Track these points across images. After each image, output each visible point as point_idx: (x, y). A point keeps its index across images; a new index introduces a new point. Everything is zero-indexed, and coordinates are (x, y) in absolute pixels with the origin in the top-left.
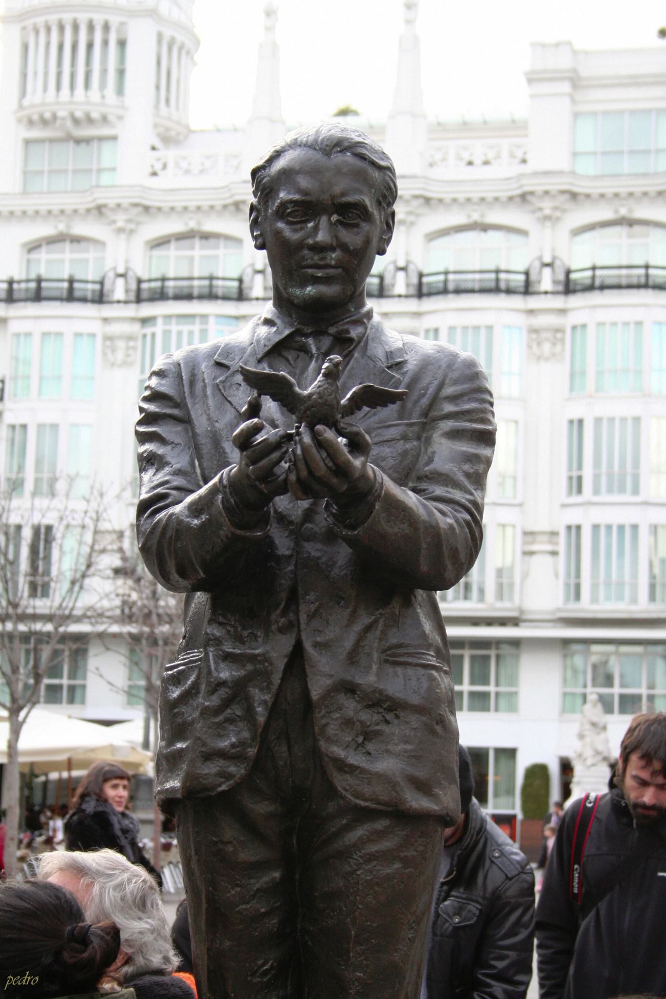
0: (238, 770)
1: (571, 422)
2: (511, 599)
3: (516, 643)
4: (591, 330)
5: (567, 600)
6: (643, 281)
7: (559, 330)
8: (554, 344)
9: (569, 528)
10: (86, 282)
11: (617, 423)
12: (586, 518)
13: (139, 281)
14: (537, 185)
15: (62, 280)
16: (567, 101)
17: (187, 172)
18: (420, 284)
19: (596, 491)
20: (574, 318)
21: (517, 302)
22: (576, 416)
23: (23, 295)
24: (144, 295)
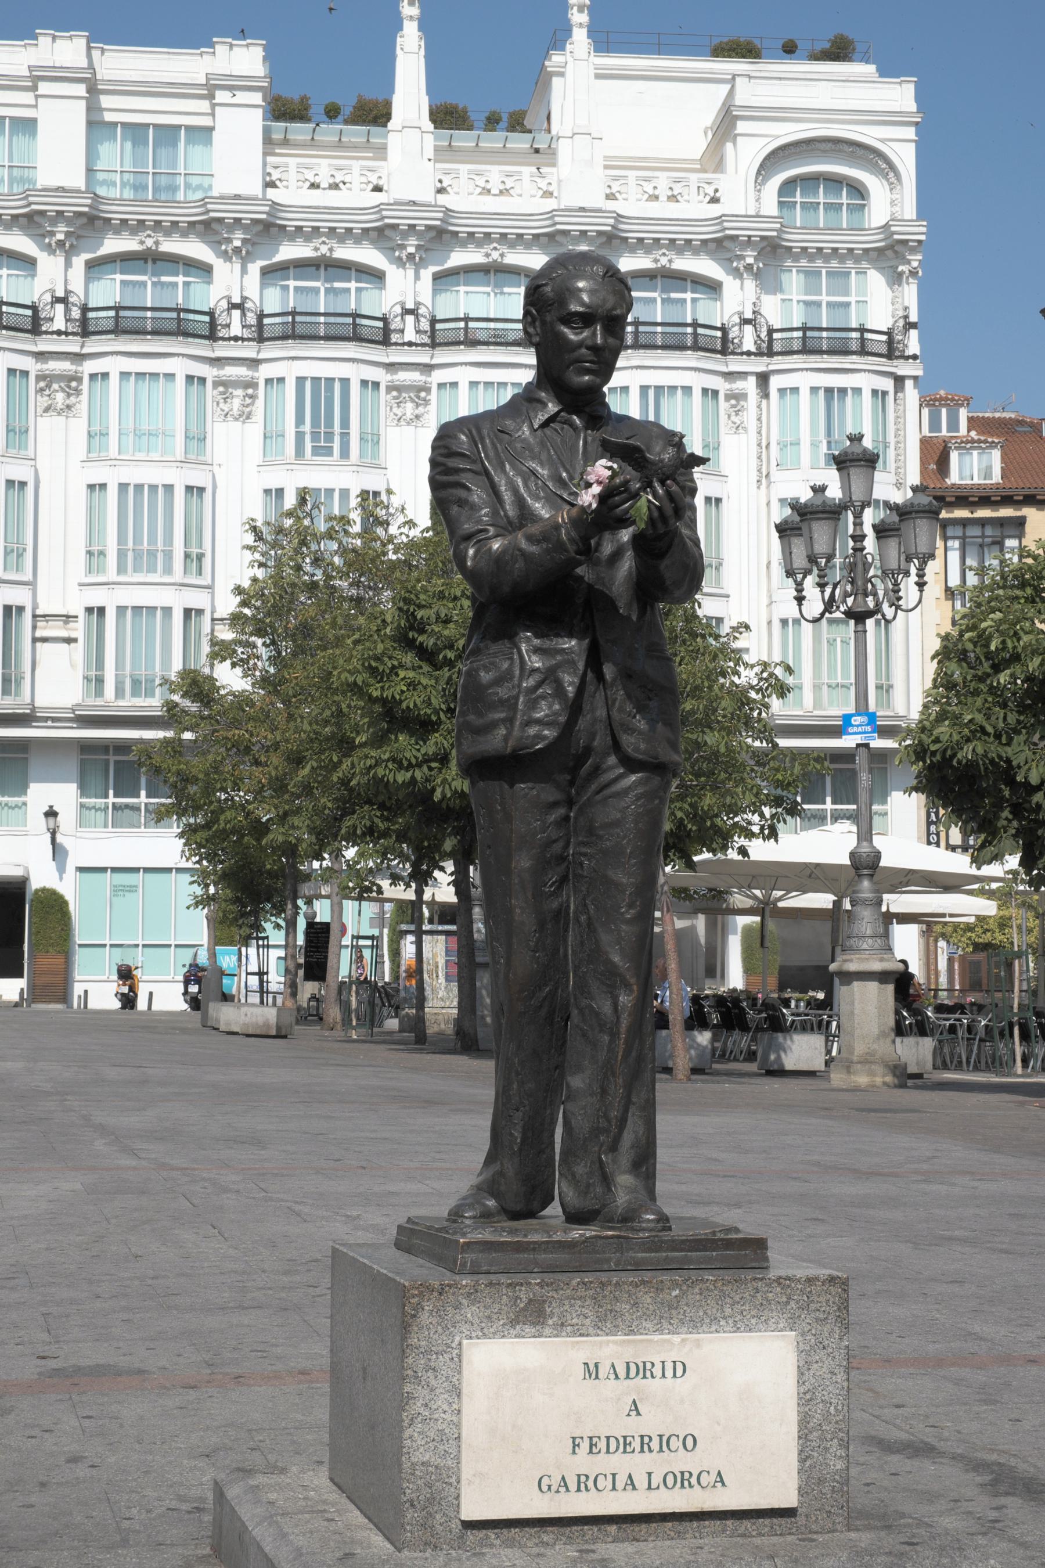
1: (267, 492)
2: (18, 694)
3: (23, 745)
4: (114, 379)
5: (87, 693)
6: (174, 326)
7: (252, 384)
8: (69, 395)
9: (89, 610)
10: (319, 314)
11: (131, 489)
12: (110, 599)
13: (771, 331)
14: (402, 218)
15: (686, 325)
16: (83, 103)
17: (314, 186)
18: (260, 325)
19: (121, 569)
20: (266, 371)
21: (201, 348)
22: (273, 485)
23: (278, 331)
24: (777, 347)
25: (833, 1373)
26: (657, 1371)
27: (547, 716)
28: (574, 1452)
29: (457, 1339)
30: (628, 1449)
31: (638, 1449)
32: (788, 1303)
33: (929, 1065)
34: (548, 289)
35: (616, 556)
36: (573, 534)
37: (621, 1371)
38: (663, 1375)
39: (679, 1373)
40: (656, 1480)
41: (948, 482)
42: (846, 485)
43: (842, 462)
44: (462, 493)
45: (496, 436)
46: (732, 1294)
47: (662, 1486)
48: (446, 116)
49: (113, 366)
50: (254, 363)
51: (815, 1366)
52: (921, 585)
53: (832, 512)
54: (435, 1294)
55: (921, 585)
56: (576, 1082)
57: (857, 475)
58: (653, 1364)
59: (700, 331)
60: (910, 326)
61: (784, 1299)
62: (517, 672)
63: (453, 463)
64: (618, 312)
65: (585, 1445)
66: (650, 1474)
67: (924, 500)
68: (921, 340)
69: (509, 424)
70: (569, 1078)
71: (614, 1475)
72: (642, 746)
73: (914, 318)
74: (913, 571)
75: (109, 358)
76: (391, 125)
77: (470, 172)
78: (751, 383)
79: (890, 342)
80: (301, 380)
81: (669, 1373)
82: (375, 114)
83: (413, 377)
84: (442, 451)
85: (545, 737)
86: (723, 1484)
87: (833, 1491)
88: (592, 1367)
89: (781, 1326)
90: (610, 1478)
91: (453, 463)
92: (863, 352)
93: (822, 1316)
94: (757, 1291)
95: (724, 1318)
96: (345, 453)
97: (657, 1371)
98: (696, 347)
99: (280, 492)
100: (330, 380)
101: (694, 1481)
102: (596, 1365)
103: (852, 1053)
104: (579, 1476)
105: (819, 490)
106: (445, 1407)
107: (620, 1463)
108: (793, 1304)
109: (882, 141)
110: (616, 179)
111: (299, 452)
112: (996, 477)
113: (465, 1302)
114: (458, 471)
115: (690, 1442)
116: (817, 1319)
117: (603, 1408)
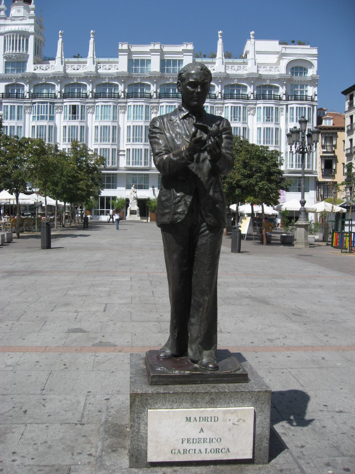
0: (183, 217)
6: (176, 96)
17: (43, 70)
20: (258, 106)
25: (265, 419)
26: (209, 420)
27: (181, 211)
28: (182, 443)
29: (147, 409)
30: (189, 442)
31: (203, 442)
32: (252, 398)
34: (184, 74)
35: (204, 160)
36: (187, 153)
37: (198, 419)
38: (211, 421)
39: (216, 420)
40: (208, 450)
41: (322, 125)
42: (301, 126)
43: (300, 122)
44: (157, 140)
45: (168, 121)
46: (234, 396)
47: (210, 453)
48: (228, 55)
49: (164, 104)
50: (223, 104)
51: (260, 417)
52: (316, 147)
53: (298, 132)
54: (140, 396)
55: (316, 147)
56: (193, 320)
57: (303, 124)
58: (208, 418)
60: (315, 95)
61: (251, 397)
62: (172, 197)
63: (154, 130)
64: (206, 81)
65: (186, 441)
66: (206, 449)
67: (316, 130)
68: (318, 98)
69: (173, 117)
70: (191, 319)
71: (195, 450)
72: (212, 221)
73: (316, 94)
74: (314, 144)
76: (216, 58)
78: (285, 107)
79: (312, 98)
81: (213, 420)
82: (214, 56)
83: (221, 105)
84: (152, 127)
85: (180, 218)
86: (229, 452)
87: (264, 452)
88: (188, 418)
89: (249, 405)
90: (194, 451)
91: (154, 130)
92: (306, 100)
93: (263, 402)
94: (242, 395)
95: (231, 403)
96: (240, 120)
97: (209, 420)
98: (242, 99)
100: (237, 107)
101: (220, 451)
102: (190, 418)
104: (184, 450)
105: (295, 127)
106: (143, 429)
107: (197, 446)
108: (253, 399)
109: (311, 60)
112: (331, 125)
113: (149, 398)
114: (156, 133)
115: (219, 440)
116: (261, 403)
117: (192, 431)
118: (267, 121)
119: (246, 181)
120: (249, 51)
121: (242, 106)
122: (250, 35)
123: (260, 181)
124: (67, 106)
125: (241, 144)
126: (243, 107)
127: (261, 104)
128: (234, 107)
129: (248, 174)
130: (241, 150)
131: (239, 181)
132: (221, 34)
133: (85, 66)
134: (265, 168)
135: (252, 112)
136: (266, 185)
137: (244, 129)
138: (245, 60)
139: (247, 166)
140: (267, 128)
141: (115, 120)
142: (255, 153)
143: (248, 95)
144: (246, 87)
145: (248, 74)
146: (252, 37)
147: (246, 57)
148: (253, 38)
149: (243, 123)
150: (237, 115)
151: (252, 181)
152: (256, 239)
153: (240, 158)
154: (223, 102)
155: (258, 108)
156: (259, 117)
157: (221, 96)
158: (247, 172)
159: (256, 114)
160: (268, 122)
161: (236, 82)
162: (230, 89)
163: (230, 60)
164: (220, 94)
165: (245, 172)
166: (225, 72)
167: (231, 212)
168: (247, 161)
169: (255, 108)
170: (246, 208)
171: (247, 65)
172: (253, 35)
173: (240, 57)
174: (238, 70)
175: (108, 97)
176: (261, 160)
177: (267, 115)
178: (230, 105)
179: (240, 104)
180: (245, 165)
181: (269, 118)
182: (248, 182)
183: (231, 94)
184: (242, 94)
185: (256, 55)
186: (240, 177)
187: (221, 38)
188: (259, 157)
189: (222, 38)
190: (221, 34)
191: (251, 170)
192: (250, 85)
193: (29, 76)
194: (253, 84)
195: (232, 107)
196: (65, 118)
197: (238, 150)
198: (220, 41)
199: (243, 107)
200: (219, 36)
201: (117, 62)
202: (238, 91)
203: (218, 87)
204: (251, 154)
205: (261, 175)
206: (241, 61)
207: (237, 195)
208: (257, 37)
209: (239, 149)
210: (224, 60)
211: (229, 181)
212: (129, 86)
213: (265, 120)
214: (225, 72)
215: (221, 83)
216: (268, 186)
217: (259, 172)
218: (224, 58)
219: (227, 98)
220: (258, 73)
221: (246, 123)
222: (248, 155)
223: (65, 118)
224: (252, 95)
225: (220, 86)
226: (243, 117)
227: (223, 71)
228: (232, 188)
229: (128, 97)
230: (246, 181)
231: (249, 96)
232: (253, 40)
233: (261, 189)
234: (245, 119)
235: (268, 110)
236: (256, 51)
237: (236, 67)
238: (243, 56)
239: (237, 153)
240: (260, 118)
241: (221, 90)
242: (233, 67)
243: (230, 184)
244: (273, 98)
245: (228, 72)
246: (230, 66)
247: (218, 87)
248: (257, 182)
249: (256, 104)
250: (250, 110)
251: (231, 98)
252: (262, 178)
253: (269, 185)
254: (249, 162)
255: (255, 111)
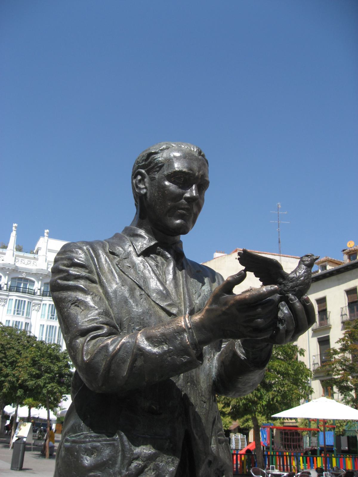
15: (15, 287)
17: (24, 263)
20: (43, 302)
33: (18, 435)
50: (8, 296)
59: (29, 290)
75: (14, 296)
76: (7, 249)
77: (33, 262)
80: (16, 300)
83: (6, 297)
96: (23, 315)
98: (28, 293)
99: (9, 321)
100: (22, 301)
103: (149, 447)
110: (29, 261)
111: (14, 313)
118: (51, 318)
119: (34, 382)
120: (41, 248)
121: (27, 300)
122: (44, 232)
123: (49, 383)
124: (46, 304)
125: (29, 339)
126: (29, 302)
127: (14, 296)
128: (19, 300)
129: (36, 374)
130: (28, 345)
131: (25, 381)
132: (16, 227)
133: (35, 262)
134: (56, 369)
135: (37, 308)
136: (55, 388)
137: (27, 324)
138: (36, 256)
139: (36, 364)
140: (50, 326)
141: (27, 317)
142: (47, 351)
143: (34, 290)
144: (34, 282)
145: (37, 270)
146: (46, 234)
147: (37, 252)
148: (47, 236)
149: (26, 318)
150: (21, 308)
151: (41, 382)
152: (35, 450)
153: (29, 354)
154: (7, 294)
155: (43, 304)
156: (43, 313)
157: (7, 288)
158: (34, 371)
159: (40, 311)
160: (52, 320)
161: (24, 275)
162: (17, 281)
163: (21, 254)
164: (6, 286)
165: (34, 371)
166: (15, 264)
167: (5, 414)
168: (37, 359)
169: (40, 304)
170: (23, 411)
171: (38, 260)
172: (48, 233)
173: (32, 252)
174: (28, 264)
175: (22, 292)
176: (52, 359)
177: (52, 313)
178: (14, 298)
179: (26, 298)
180: (34, 363)
181: (54, 316)
182: (35, 383)
183: (17, 287)
184: (29, 289)
185: (48, 253)
186: (26, 377)
187: (15, 230)
188: (50, 355)
189: (17, 231)
190: (16, 227)
191: (39, 369)
192: (38, 280)
193: (10, 268)
194: (41, 280)
195: (16, 300)
196: (43, 316)
197: (25, 346)
198: (13, 234)
199: (28, 302)
200: (14, 228)
201: (4, 254)
202: (25, 285)
203: (38, 283)
204: (41, 351)
205: (51, 375)
206: (32, 256)
207: (18, 396)
208: (51, 236)
209: (27, 345)
210: (15, 252)
211: (12, 380)
212: (12, 279)
213: (49, 318)
214: (15, 264)
215: (8, 275)
216: (58, 389)
217: (49, 373)
218: (15, 250)
219: (13, 290)
220: (47, 270)
221: (29, 318)
222: (38, 352)
223: (43, 316)
224: (39, 291)
225: (7, 277)
226: (27, 312)
227: (12, 262)
228: (13, 388)
229: (10, 290)
230: (34, 382)
231: (35, 291)
232: (46, 238)
233: (49, 392)
234: (28, 314)
235: (19, 304)
236: (48, 249)
237: (26, 261)
238: (35, 251)
239: (24, 349)
240: (44, 315)
241: (41, 286)
242: (23, 260)
243: (12, 383)
244: (27, 292)
245: (17, 264)
246: (20, 259)
247: (38, 283)
248: (45, 383)
249: (41, 301)
250: (35, 305)
251: (16, 291)
252: (52, 379)
253: (59, 388)
254: (39, 360)
255: (40, 307)
